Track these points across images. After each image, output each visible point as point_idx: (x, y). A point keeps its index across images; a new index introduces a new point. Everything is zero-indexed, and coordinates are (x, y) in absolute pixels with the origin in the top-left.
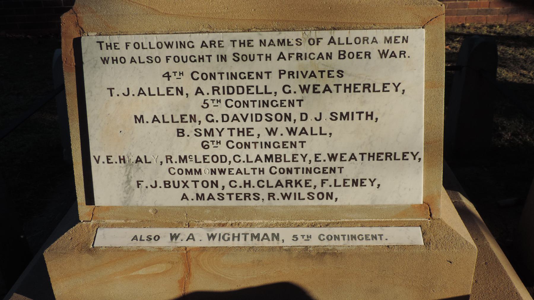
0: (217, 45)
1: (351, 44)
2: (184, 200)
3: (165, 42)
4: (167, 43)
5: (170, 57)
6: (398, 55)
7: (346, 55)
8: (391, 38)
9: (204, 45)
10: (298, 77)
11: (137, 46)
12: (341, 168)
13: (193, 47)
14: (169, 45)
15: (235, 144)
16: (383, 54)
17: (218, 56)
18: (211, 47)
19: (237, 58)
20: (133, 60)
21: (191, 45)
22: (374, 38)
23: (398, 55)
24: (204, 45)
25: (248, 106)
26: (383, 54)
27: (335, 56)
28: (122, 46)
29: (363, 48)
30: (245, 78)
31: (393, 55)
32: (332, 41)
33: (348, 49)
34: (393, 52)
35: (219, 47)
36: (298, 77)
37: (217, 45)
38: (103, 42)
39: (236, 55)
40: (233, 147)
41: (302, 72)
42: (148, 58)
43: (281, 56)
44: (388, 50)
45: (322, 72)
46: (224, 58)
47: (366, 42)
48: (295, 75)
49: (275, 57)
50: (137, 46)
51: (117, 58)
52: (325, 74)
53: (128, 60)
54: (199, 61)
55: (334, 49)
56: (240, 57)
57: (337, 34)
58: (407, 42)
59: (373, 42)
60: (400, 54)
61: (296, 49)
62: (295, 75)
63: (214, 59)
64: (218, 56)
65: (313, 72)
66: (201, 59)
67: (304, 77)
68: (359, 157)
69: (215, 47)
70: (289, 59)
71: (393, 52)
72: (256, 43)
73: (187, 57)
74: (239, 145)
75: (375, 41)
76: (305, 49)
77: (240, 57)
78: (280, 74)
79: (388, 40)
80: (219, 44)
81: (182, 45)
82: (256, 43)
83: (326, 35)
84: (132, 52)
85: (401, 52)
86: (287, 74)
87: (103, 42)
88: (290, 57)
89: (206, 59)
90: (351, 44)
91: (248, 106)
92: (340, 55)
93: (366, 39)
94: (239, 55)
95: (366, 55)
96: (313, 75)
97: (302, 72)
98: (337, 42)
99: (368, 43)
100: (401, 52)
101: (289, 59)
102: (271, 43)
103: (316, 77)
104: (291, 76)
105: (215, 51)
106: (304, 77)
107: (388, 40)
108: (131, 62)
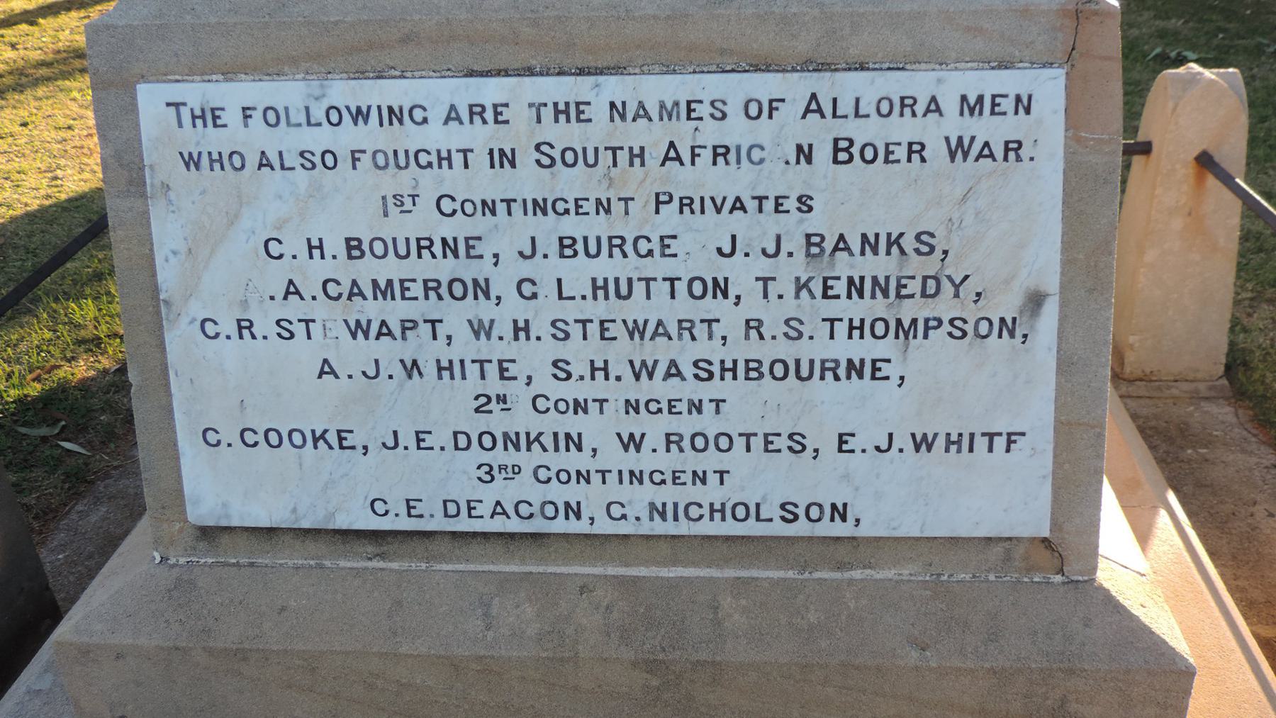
0: (489, 115)
1: (868, 116)
2: (451, 123)
3: (348, 108)
4: (354, 111)
5: (364, 152)
6: (999, 152)
7: (855, 150)
8: (980, 99)
9: (452, 116)
10: (703, 212)
11: (274, 117)
12: (718, 402)
13: (534, 296)
14: (360, 115)
15: (552, 474)
16: (957, 149)
17: (491, 152)
18: (471, 122)
19: (547, 158)
20: (264, 163)
21: (418, 115)
22: (933, 99)
23: (999, 152)
24: (452, 116)
25: (493, 213)
26: (957, 149)
27: (823, 153)
28: (232, 116)
29: (903, 129)
30: (567, 211)
31: (986, 152)
32: (813, 106)
33: (862, 132)
34: (986, 144)
35: (496, 122)
36: (703, 212)
37: (489, 115)
38: (184, 104)
39: (545, 148)
40: (549, 480)
41: (713, 199)
42: (302, 154)
43: (672, 155)
44: (973, 138)
45: (761, 199)
46: (504, 158)
47: (907, 111)
48: (697, 206)
49: (655, 153)
50: (274, 117)
51: (220, 154)
52: (769, 205)
53: (253, 160)
54: (440, 167)
55: (820, 133)
56: (556, 154)
57: (825, 85)
58: (1028, 111)
59: (928, 111)
60: (1007, 150)
61: (711, 133)
62: (697, 206)
63: (479, 159)
64: (491, 152)
65: (738, 199)
66: (445, 159)
67: (719, 211)
68: (751, 205)
69: (485, 122)
70: (693, 163)
71: (986, 144)
72: (599, 111)
73: (407, 152)
74: (564, 477)
75: (934, 107)
76: (736, 131)
77: (556, 154)
78: (658, 203)
79: (971, 107)
80: (497, 114)
81: (394, 115)
82: (599, 111)
83: (794, 88)
84: (258, 138)
85: (1007, 143)
86: (676, 203)
87: (184, 104)
88: (694, 155)
89: (457, 159)
90: (868, 116)
91: (493, 213)
92: (836, 150)
93: (907, 104)
94: (552, 147)
95: (910, 152)
96: (738, 205)
97: (713, 199)
98: (828, 110)
99: (914, 114)
100: (1007, 143)
101: (693, 163)
102: (643, 112)
103: (745, 212)
104: (686, 209)
105: (480, 136)
106: (719, 211)
107: (971, 107)
108: (261, 166)
